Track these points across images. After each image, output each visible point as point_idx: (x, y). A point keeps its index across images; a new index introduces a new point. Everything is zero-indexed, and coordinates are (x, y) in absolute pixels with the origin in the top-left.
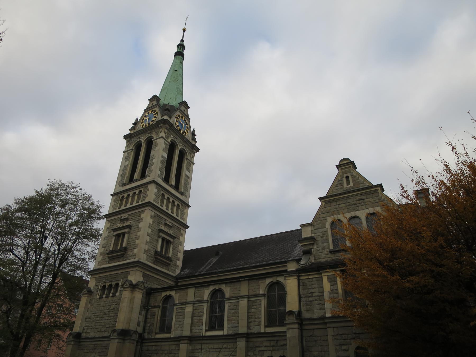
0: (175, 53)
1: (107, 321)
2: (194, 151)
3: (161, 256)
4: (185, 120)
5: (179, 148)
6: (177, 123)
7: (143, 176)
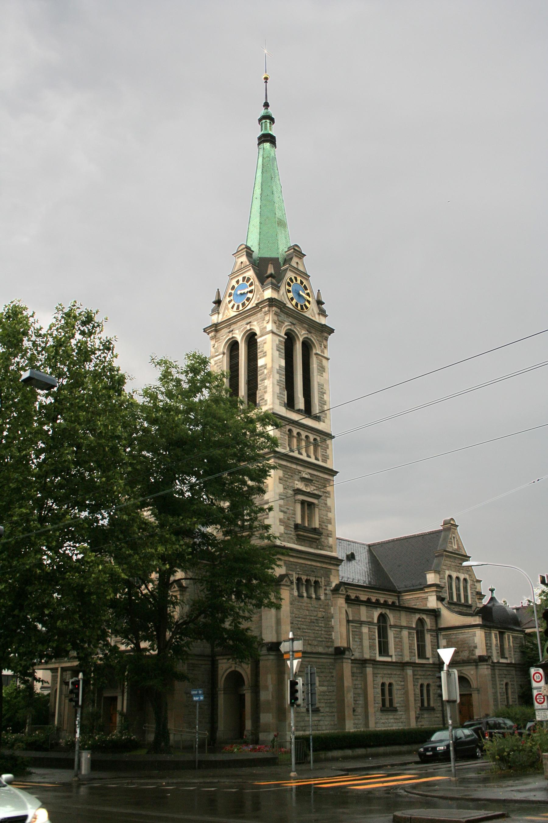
0: (259, 138)
1: (317, 632)
2: (326, 335)
3: (305, 529)
4: (302, 282)
5: (301, 339)
6: (291, 295)
7: (233, 346)
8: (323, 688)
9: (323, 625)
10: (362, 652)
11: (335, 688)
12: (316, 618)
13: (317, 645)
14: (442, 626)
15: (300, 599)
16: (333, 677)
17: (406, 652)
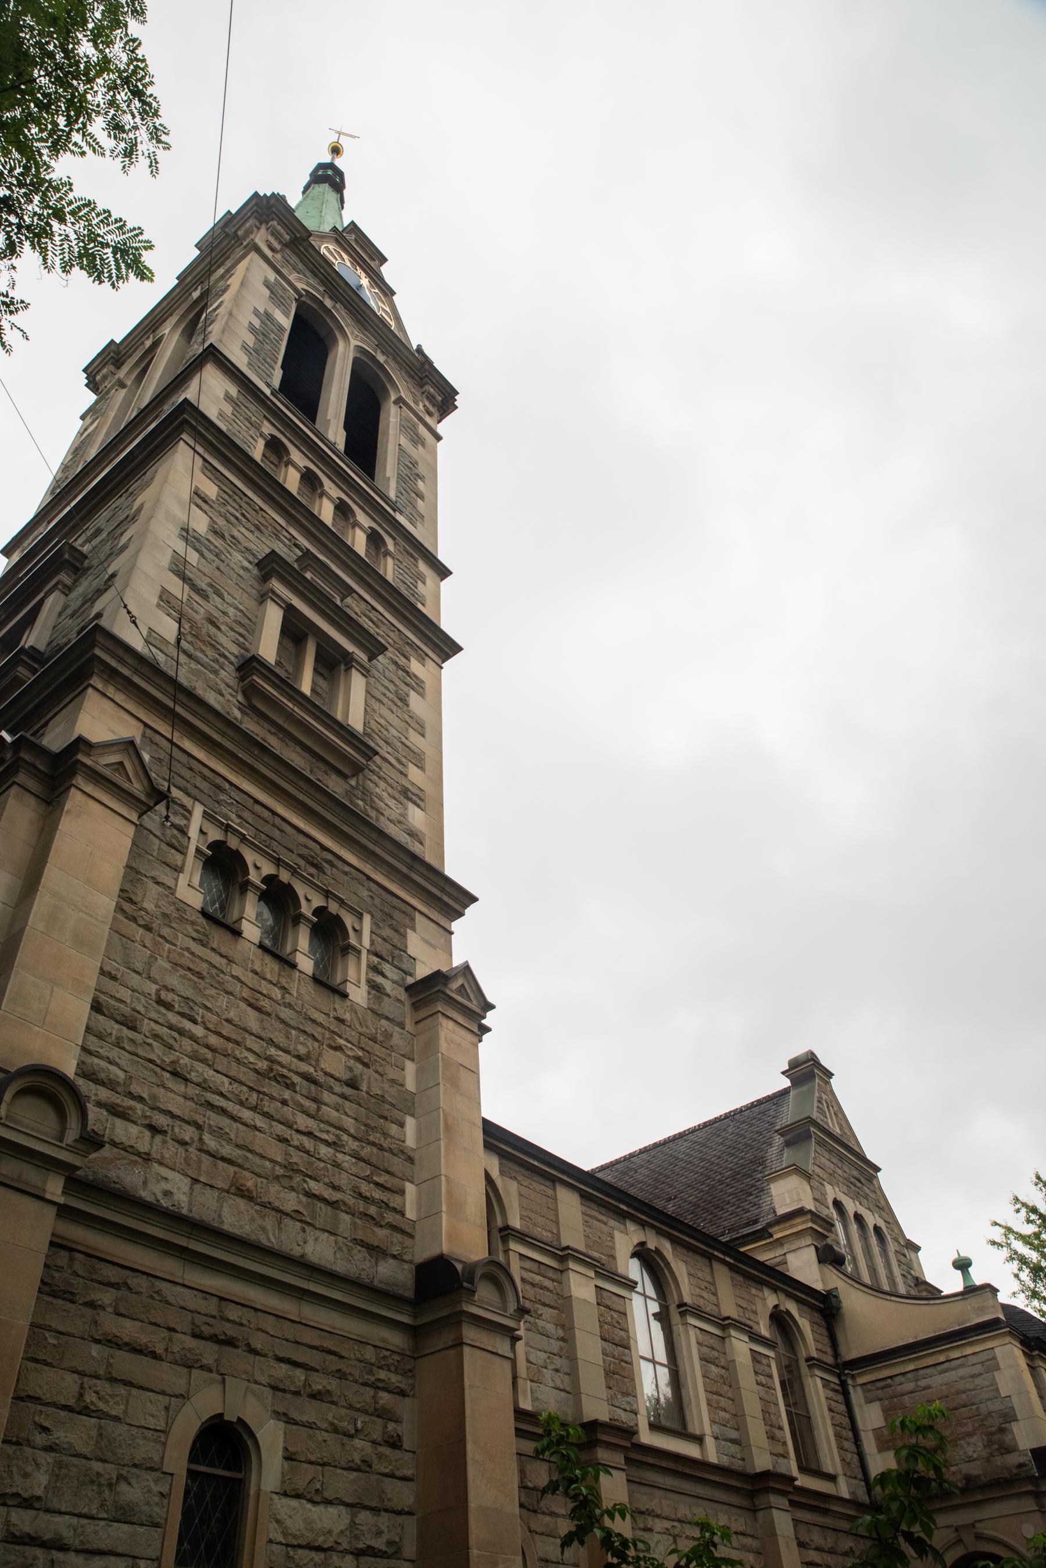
8: (316, 1512)
9: (349, 1123)
10: (574, 1392)
11: (411, 1525)
12: (304, 1067)
13: (295, 1215)
14: (854, 1354)
15: (218, 937)
16: (395, 1443)
17: (757, 1431)
